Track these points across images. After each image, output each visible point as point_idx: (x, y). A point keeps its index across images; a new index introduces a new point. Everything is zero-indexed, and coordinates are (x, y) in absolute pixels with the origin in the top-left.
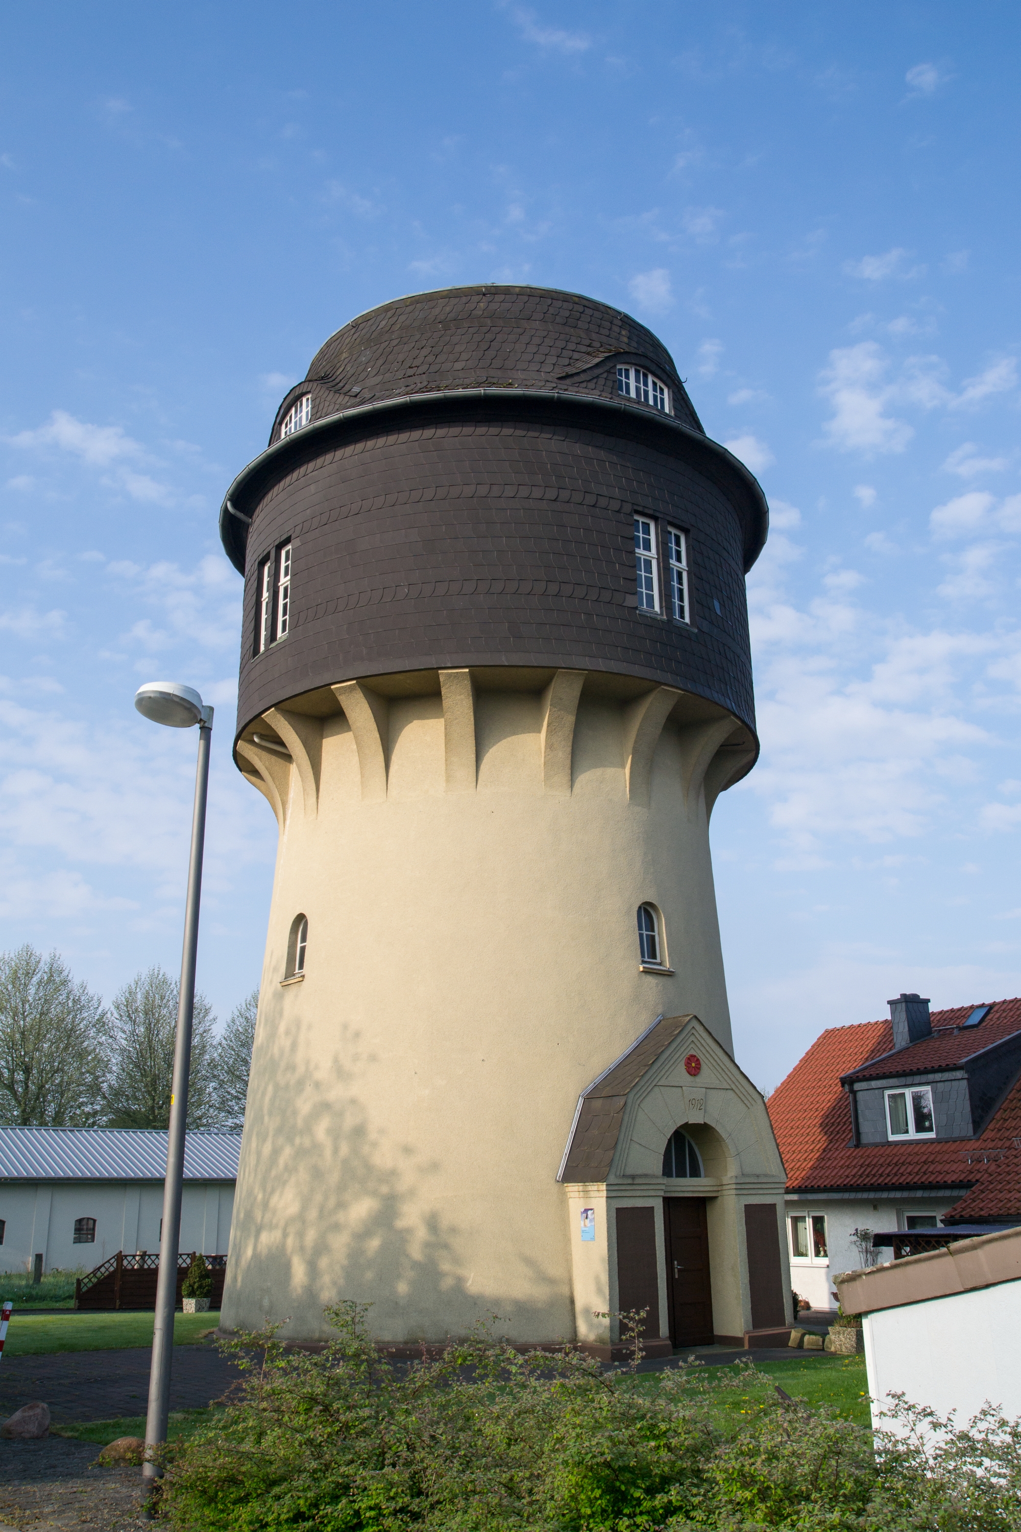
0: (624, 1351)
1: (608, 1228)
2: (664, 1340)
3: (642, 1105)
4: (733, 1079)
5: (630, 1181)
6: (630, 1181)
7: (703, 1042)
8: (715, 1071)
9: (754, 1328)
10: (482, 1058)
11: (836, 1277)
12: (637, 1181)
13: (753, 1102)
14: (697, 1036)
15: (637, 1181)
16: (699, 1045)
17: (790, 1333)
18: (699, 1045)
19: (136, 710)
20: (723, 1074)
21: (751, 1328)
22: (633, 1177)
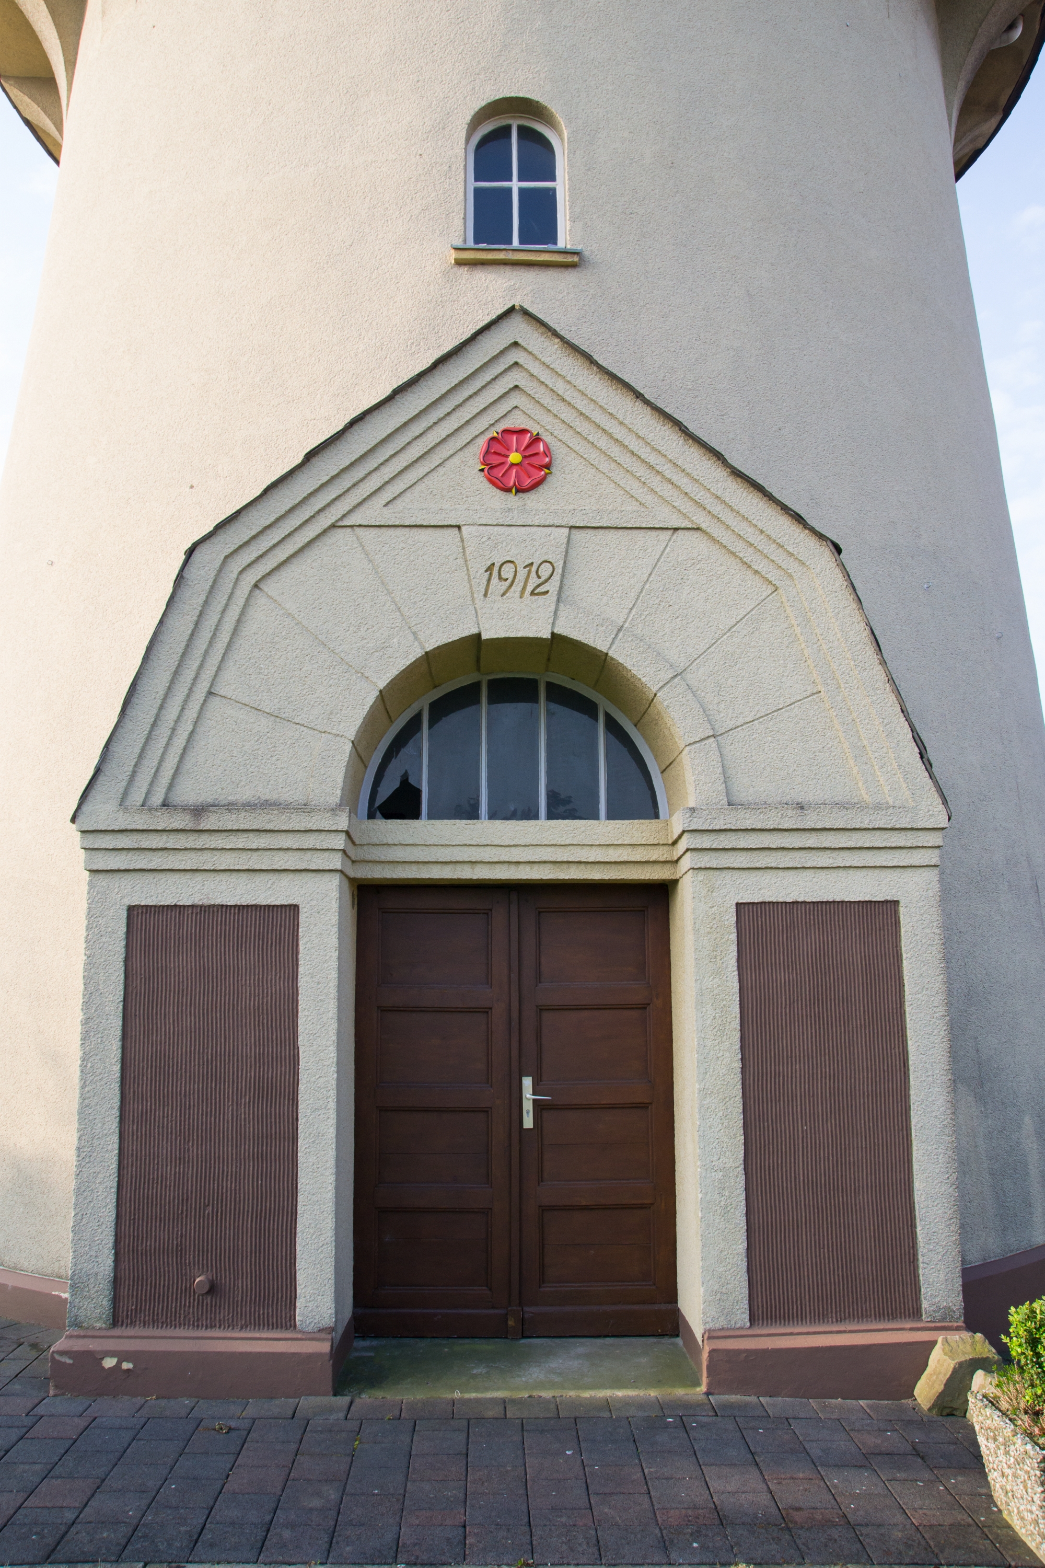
0: (109, 1363)
1: (91, 964)
2: (310, 1337)
3: (270, 587)
4: (700, 495)
5: (181, 821)
6: (181, 821)
7: (560, 387)
8: (619, 476)
9: (753, 1319)
10: (188, 489)
11: (710, 1330)
12: (211, 822)
13: (792, 566)
14: (535, 368)
15: (211, 822)
16: (547, 400)
17: (932, 1344)
18: (547, 400)
19: (541, 100)
20: (655, 482)
21: (742, 1317)
22: (199, 811)
